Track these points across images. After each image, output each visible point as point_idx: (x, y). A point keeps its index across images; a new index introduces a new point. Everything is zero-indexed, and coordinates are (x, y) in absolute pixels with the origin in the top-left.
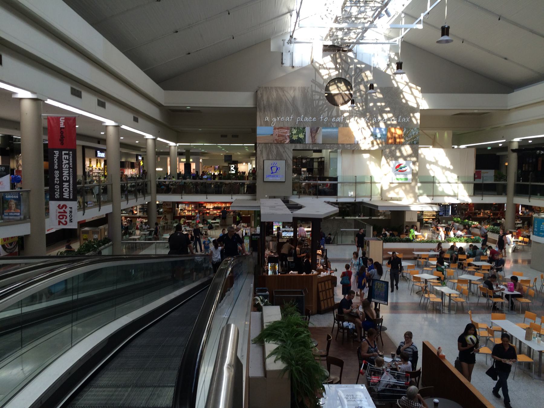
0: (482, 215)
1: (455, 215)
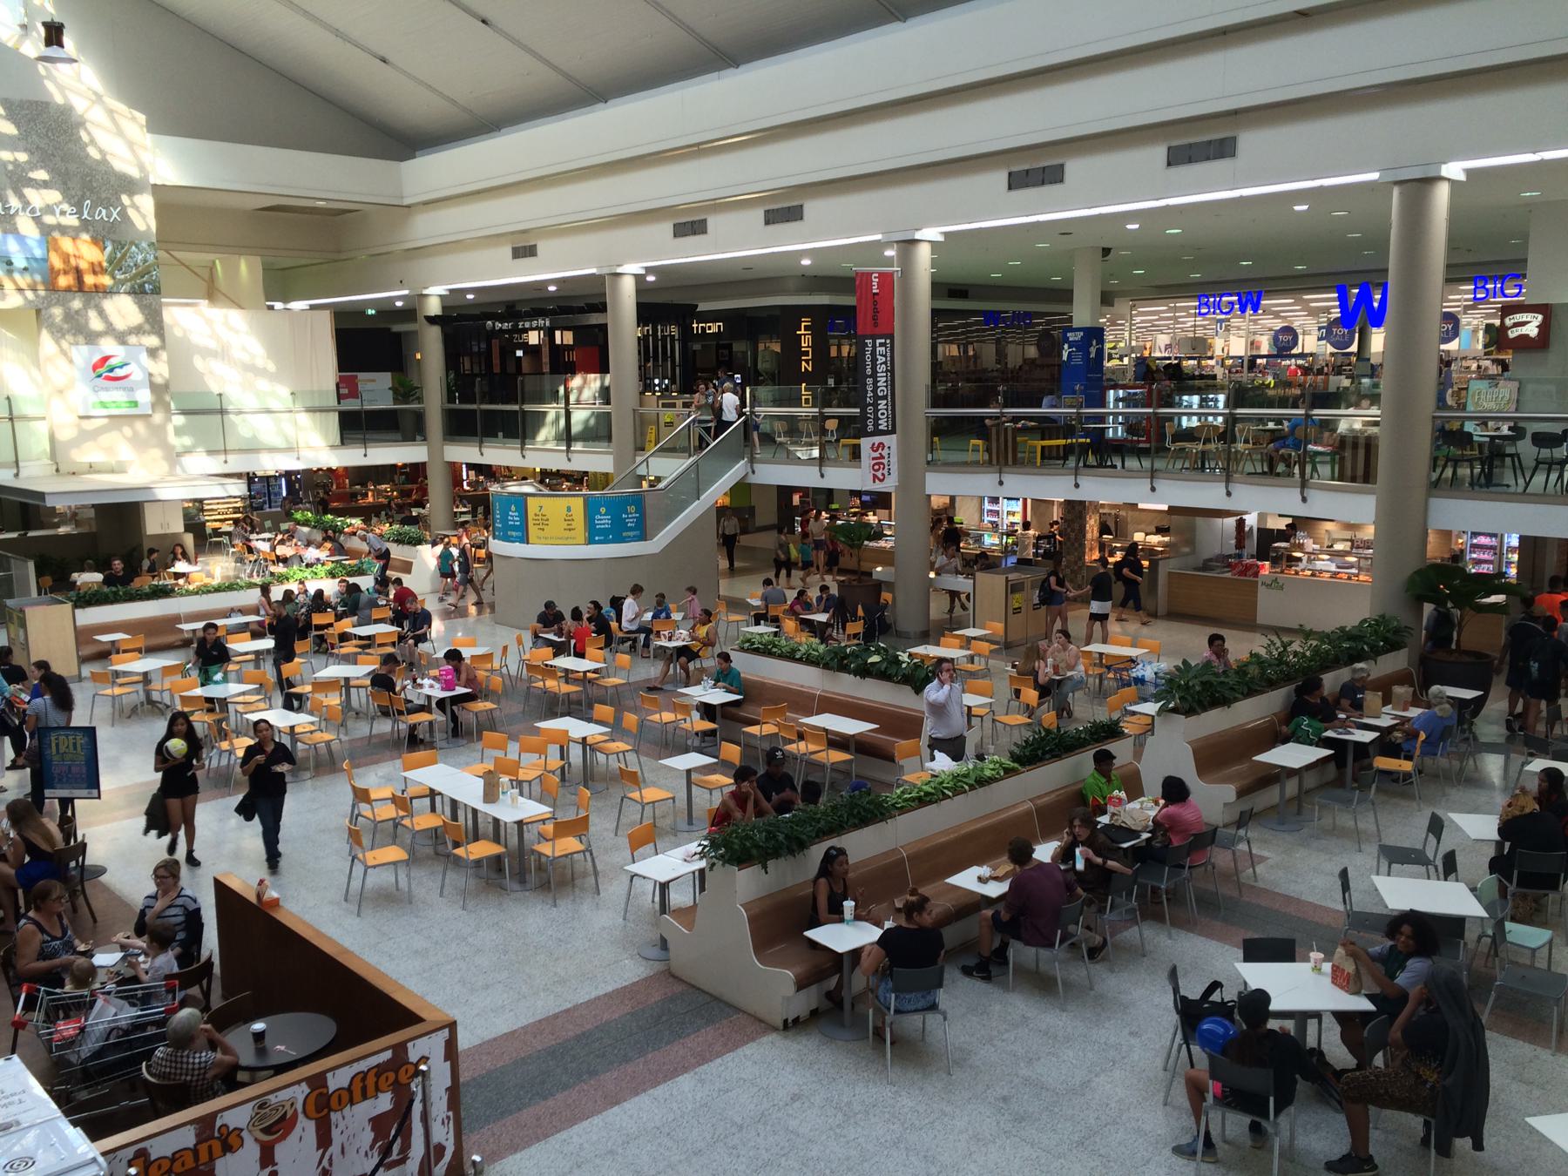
0: (370, 499)
1: (298, 504)
